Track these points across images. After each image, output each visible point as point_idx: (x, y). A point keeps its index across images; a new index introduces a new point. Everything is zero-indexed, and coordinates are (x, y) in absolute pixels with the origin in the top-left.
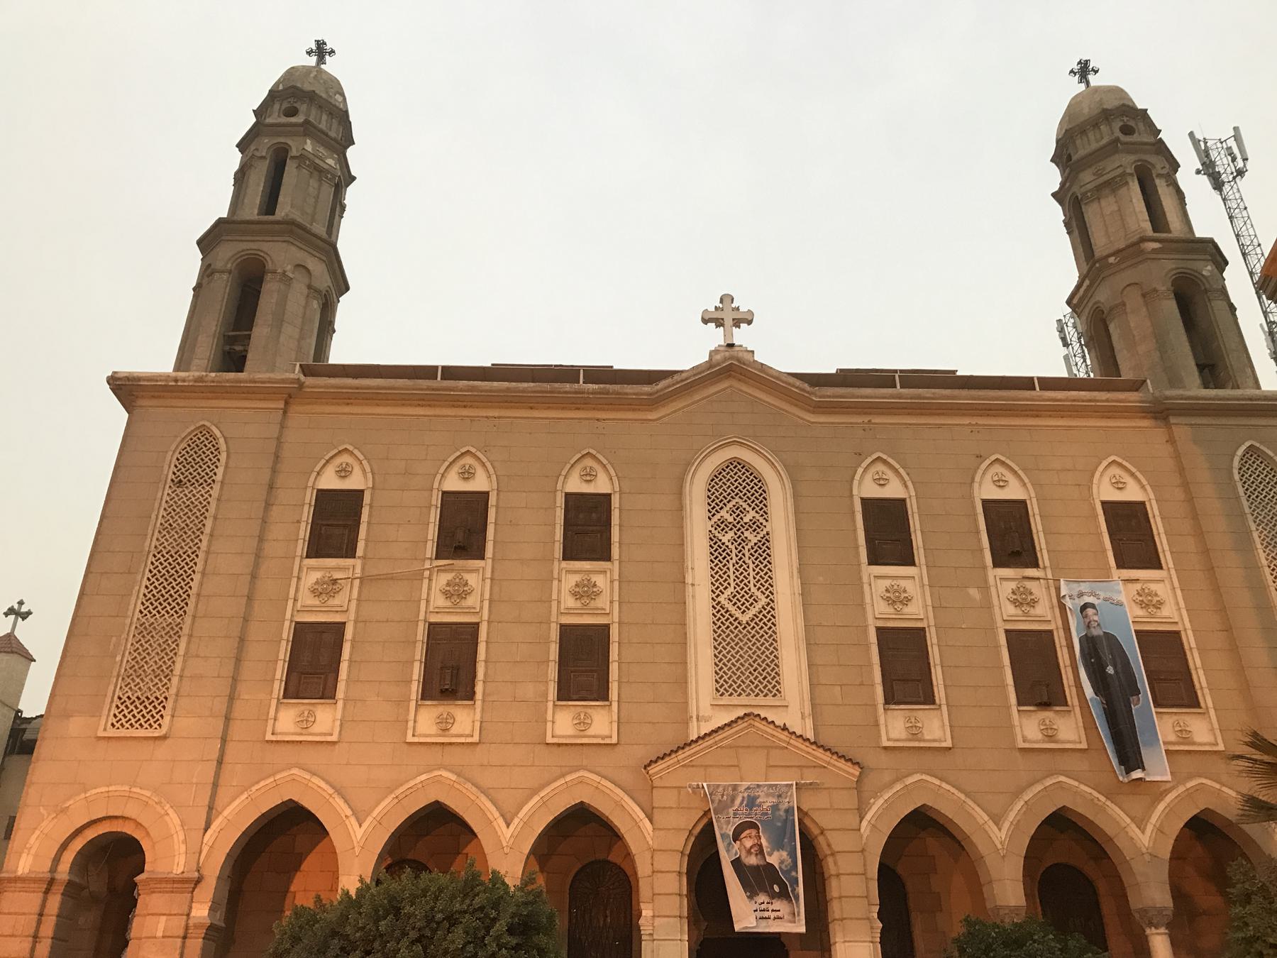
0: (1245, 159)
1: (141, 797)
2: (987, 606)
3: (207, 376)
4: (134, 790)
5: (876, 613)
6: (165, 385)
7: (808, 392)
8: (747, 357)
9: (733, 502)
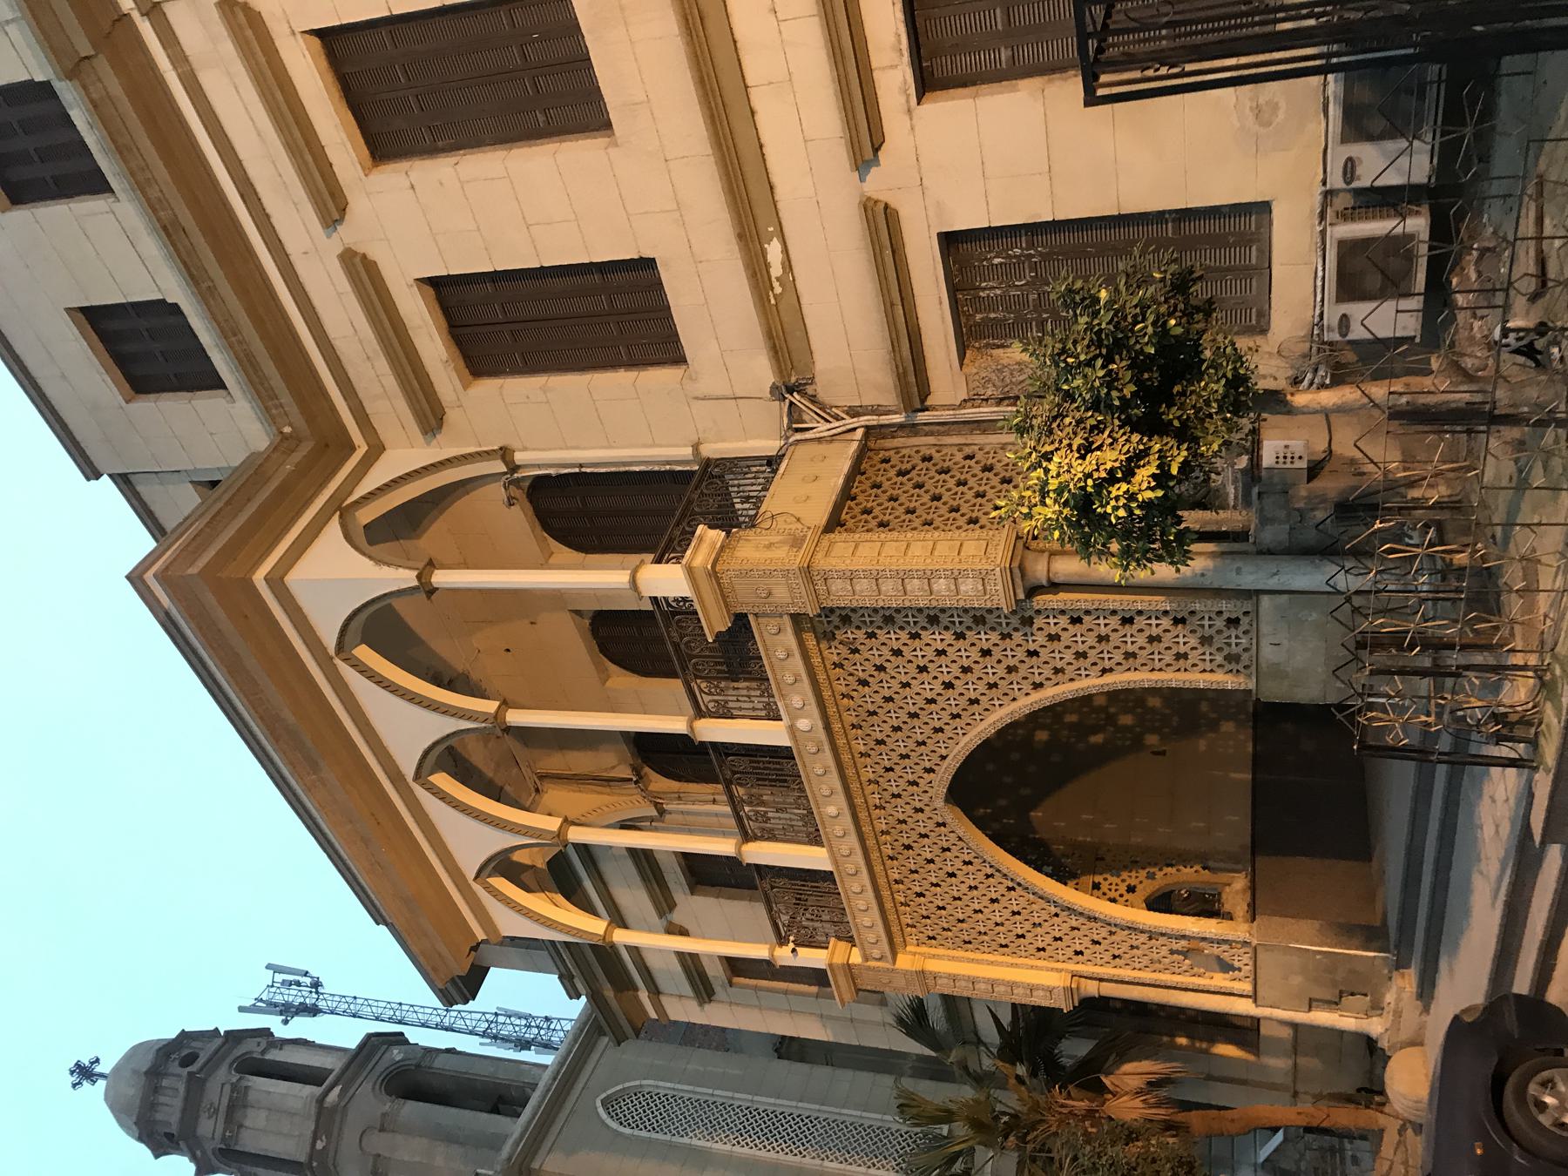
0: (306, 974)
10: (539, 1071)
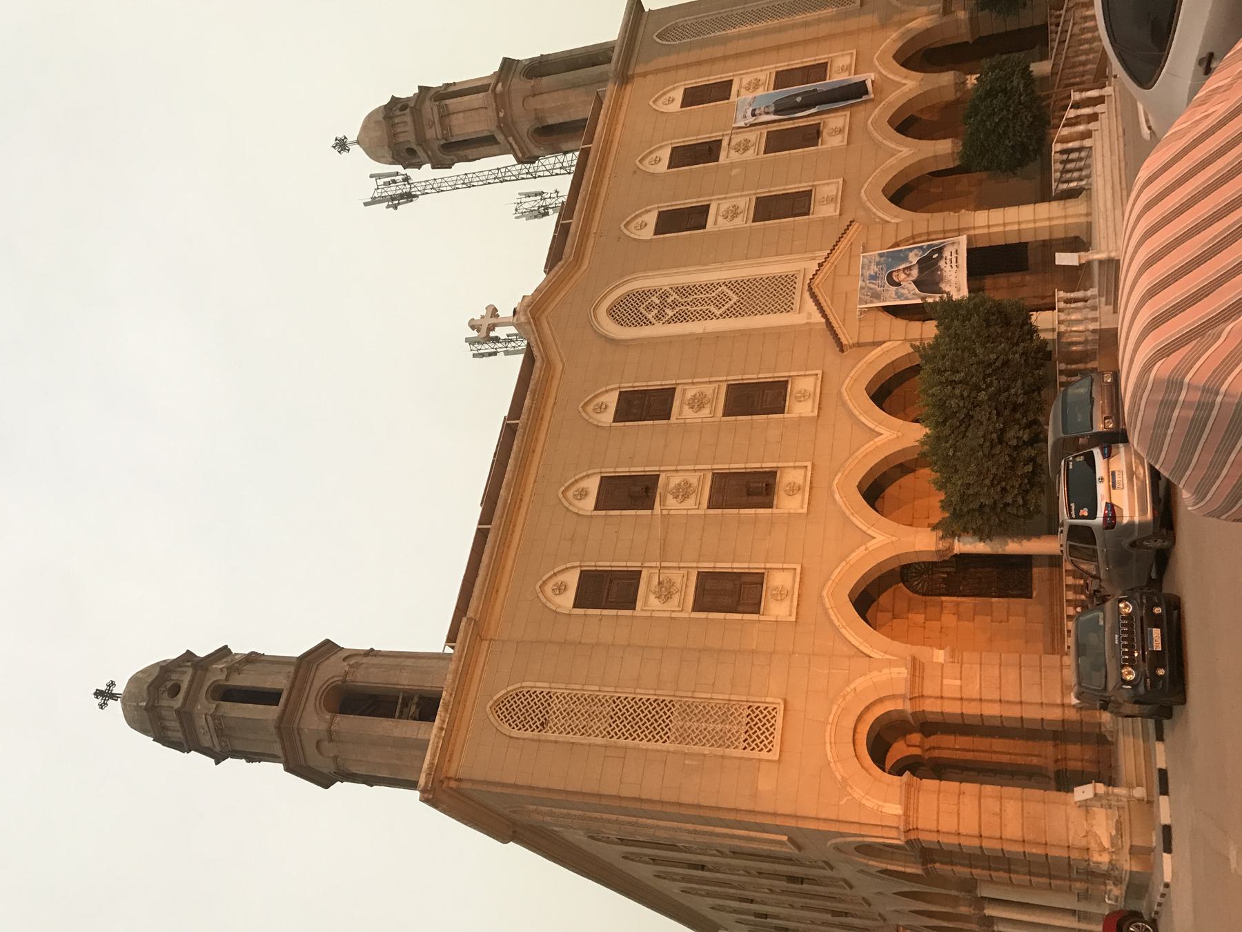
2: (744, 165)
4: (830, 721)
5: (677, 609)
7: (565, 263)
8: (526, 300)
9: (643, 311)
10: (442, 663)
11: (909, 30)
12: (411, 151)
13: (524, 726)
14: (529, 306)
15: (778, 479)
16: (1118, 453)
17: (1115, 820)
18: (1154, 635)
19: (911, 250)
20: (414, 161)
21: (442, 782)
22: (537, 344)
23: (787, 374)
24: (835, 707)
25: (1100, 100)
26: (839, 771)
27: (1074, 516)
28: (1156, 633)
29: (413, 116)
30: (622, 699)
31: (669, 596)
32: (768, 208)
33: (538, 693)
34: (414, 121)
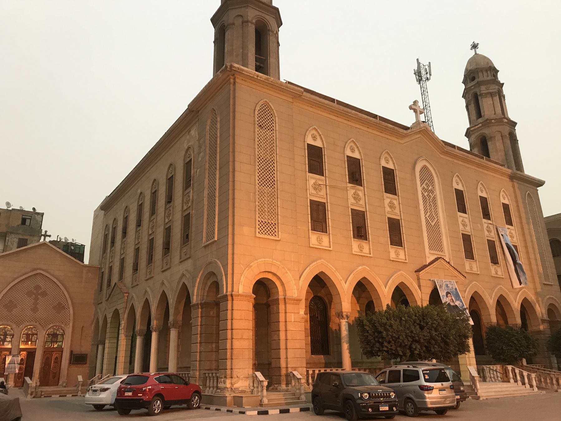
0: (430, 75)
1: (277, 265)
2: (482, 230)
3: (270, 78)
6: (252, 77)
9: (425, 182)
11: (535, 304)
12: (473, 79)
13: (259, 117)
14: (426, 129)
15: (364, 241)
16: (451, 393)
17: (245, 390)
18: (386, 407)
19: (461, 302)
20: (468, 80)
21: (233, 75)
22: (412, 132)
23: (406, 246)
24: (279, 263)
25: (531, 386)
26: (254, 264)
27: (424, 372)
28: (387, 408)
29: (491, 80)
30: (274, 165)
31: (315, 189)
32: (467, 239)
33: (273, 124)
34: (489, 80)
